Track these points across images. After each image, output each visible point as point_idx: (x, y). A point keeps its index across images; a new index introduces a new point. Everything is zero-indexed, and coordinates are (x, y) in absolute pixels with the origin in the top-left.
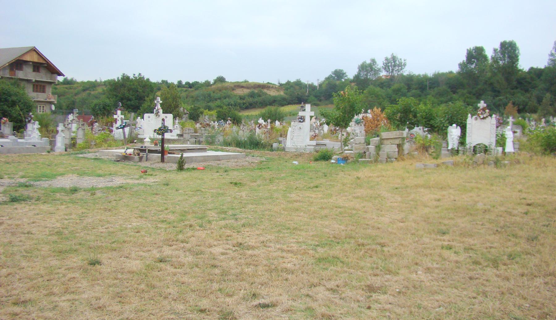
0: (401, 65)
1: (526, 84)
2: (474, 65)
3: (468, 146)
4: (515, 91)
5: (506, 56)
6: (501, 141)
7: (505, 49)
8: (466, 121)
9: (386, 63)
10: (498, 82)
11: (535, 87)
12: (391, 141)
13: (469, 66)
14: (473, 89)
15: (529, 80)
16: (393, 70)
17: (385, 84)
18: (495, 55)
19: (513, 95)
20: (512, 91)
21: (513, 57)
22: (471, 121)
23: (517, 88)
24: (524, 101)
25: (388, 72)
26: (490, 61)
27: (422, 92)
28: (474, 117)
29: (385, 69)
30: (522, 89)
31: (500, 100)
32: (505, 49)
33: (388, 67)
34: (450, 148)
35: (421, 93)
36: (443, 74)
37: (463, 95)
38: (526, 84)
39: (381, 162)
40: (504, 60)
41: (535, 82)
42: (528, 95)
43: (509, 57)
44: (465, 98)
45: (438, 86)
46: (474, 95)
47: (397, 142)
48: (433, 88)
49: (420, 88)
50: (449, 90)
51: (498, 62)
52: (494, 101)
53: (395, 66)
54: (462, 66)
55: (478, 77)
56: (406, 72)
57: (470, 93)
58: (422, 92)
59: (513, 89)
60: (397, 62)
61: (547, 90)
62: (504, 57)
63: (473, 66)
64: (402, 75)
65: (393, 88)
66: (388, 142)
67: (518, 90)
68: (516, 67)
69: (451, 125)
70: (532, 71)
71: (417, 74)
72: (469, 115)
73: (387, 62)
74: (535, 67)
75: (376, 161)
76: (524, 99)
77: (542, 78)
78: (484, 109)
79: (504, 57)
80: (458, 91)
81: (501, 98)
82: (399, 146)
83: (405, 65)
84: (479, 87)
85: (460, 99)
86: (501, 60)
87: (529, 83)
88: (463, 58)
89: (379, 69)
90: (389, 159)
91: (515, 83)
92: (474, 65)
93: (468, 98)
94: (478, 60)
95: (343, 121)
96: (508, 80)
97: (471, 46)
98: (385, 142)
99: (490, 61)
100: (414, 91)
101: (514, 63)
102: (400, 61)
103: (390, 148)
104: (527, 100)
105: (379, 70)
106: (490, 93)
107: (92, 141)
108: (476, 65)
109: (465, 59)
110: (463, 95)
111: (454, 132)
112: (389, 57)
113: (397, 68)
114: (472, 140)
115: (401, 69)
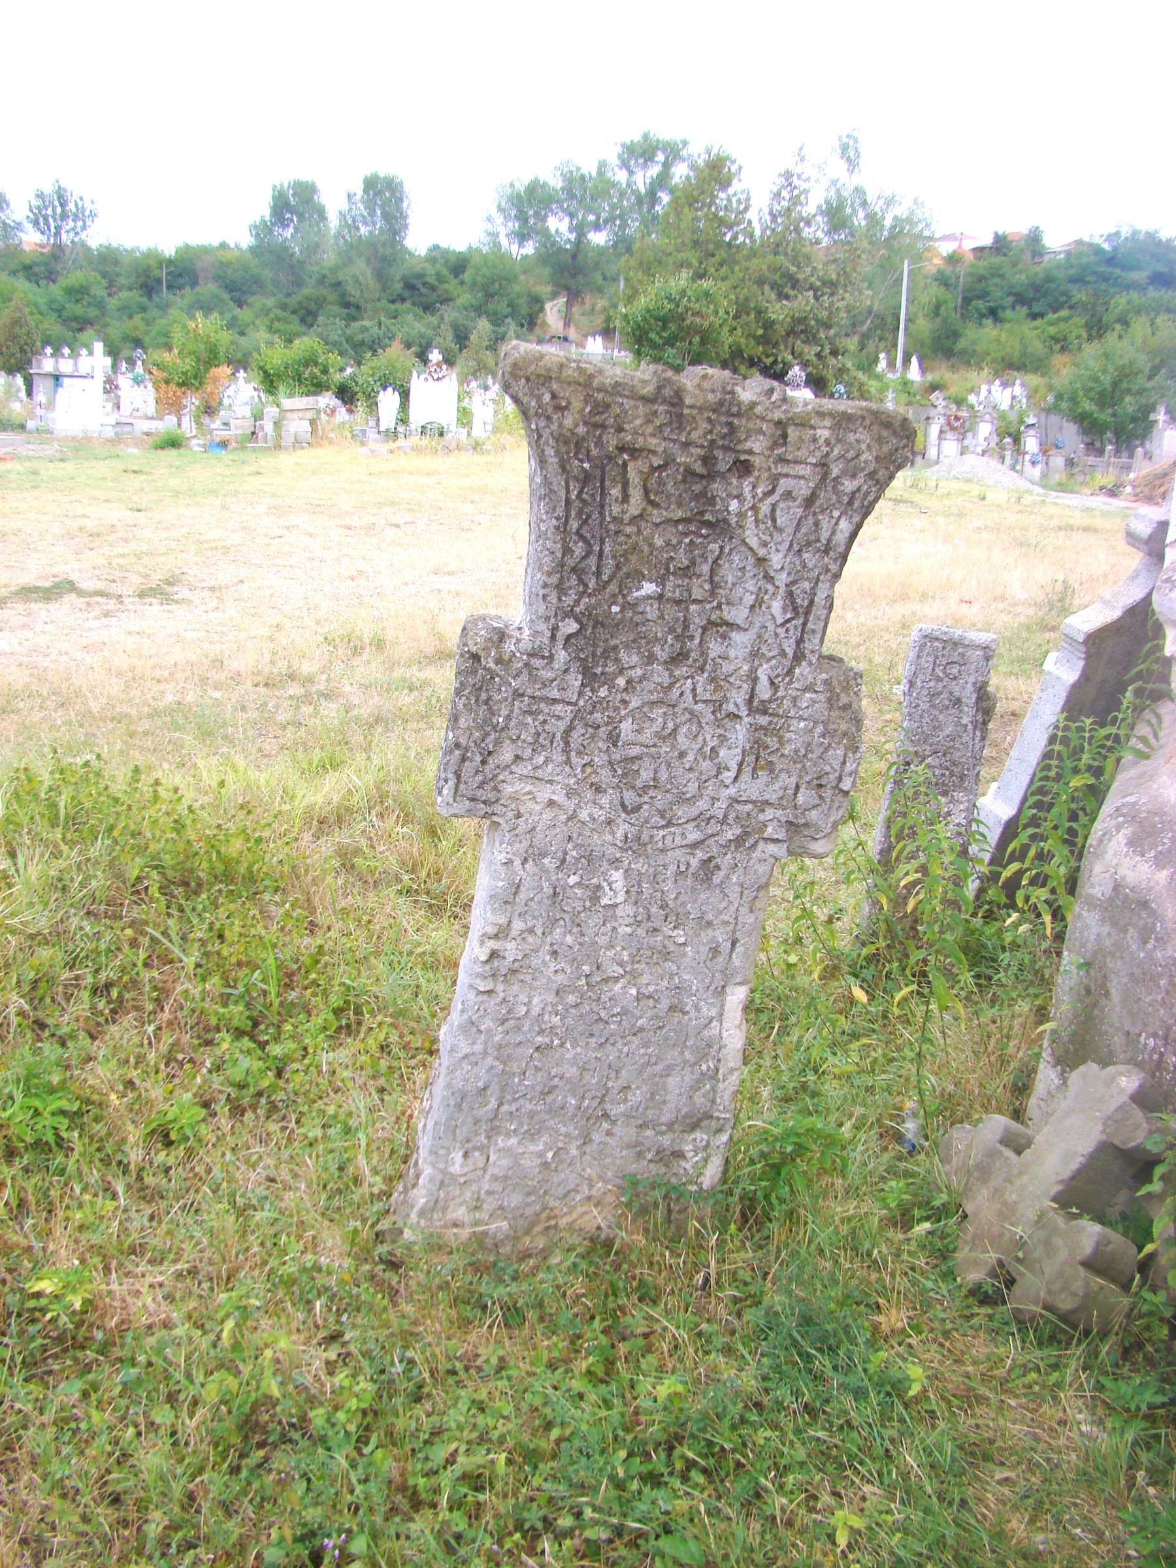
0: (82, 216)
1: (424, 290)
2: (291, 230)
3: (413, 427)
4: (398, 306)
5: (379, 212)
6: (465, 417)
7: (376, 194)
8: (409, 382)
9: (39, 208)
10: (357, 282)
11: (447, 300)
12: (301, 414)
13: (277, 230)
14: (288, 295)
15: (431, 280)
16: (58, 229)
17: (36, 269)
18: (350, 210)
19: (395, 317)
20: (392, 307)
21: (395, 218)
22: (419, 385)
23: (403, 300)
24: (422, 336)
25: (43, 233)
26: (334, 222)
27: (150, 297)
28: (423, 377)
29: (36, 223)
30: (414, 304)
31: (364, 329)
32: (376, 194)
33: (46, 218)
34: (382, 429)
35: (145, 299)
36: (205, 251)
37: (266, 312)
38: (424, 290)
39: (286, 448)
40: (374, 224)
41: (446, 286)
42: (434, 320)
43: (386, 216)
44: (272, 321)
45: (194, 284)
46: (294, 312)
47: (310, 415)
48: (181, 288)
49: (141, 287)
50: (226, 296)
51: (358, 229)
52: (348, 332)
53: (64, 217)
54: (262, 231)
55: (301, 263)
56: (96, 237)
57: (284, 307)
58: (150, 297)
59: (393, 302)
60: (71, 206)
61: (479, 310)
62: (372, 213)
63: (289, 232)
64: (83, 244)
65: (63, 282)
66: (295, 415)
67: (407, 305)
68: (401, 243)
69: (385, 389)
70: (437, 254)
71: (129, 246)
72: (415, 374)
73: (40, 203)
74: (444, 245)
75: (278, 447)
76: (423, 330)
77: (467, 276)
78: (439, 365)
79: (372, 213)
80: (251, 300)
81: (366, 323)
82: (313, 422)
83: (93, 215)
84: (307, 291)
85: (258, 322)
86: (365, 224)
87: (433, 288)
88: (263, 209)
89: (20, 224)
90: (298, 443)
91: (398, 287)
92: (291, 230)
93: (279, 320)
94: (301, 217)
95: (195, 378)
96: (380, 275)
97: (286, 176)
98: (288, 415)
99: (334, 222)
100: (124, 294)
101: (395, 233)
102: (80, 204)
103: (298, 426)
104: (430, 333)
105: (19, 226)
106: (336, 309)
107: (818, 384)
108: (296, 230)
109: (267, 214)
110: (266, 312)
111: (388, 401)
112: (49, 189)
113: (71, 224)
114: (419, 414)
115: (84, 228)
